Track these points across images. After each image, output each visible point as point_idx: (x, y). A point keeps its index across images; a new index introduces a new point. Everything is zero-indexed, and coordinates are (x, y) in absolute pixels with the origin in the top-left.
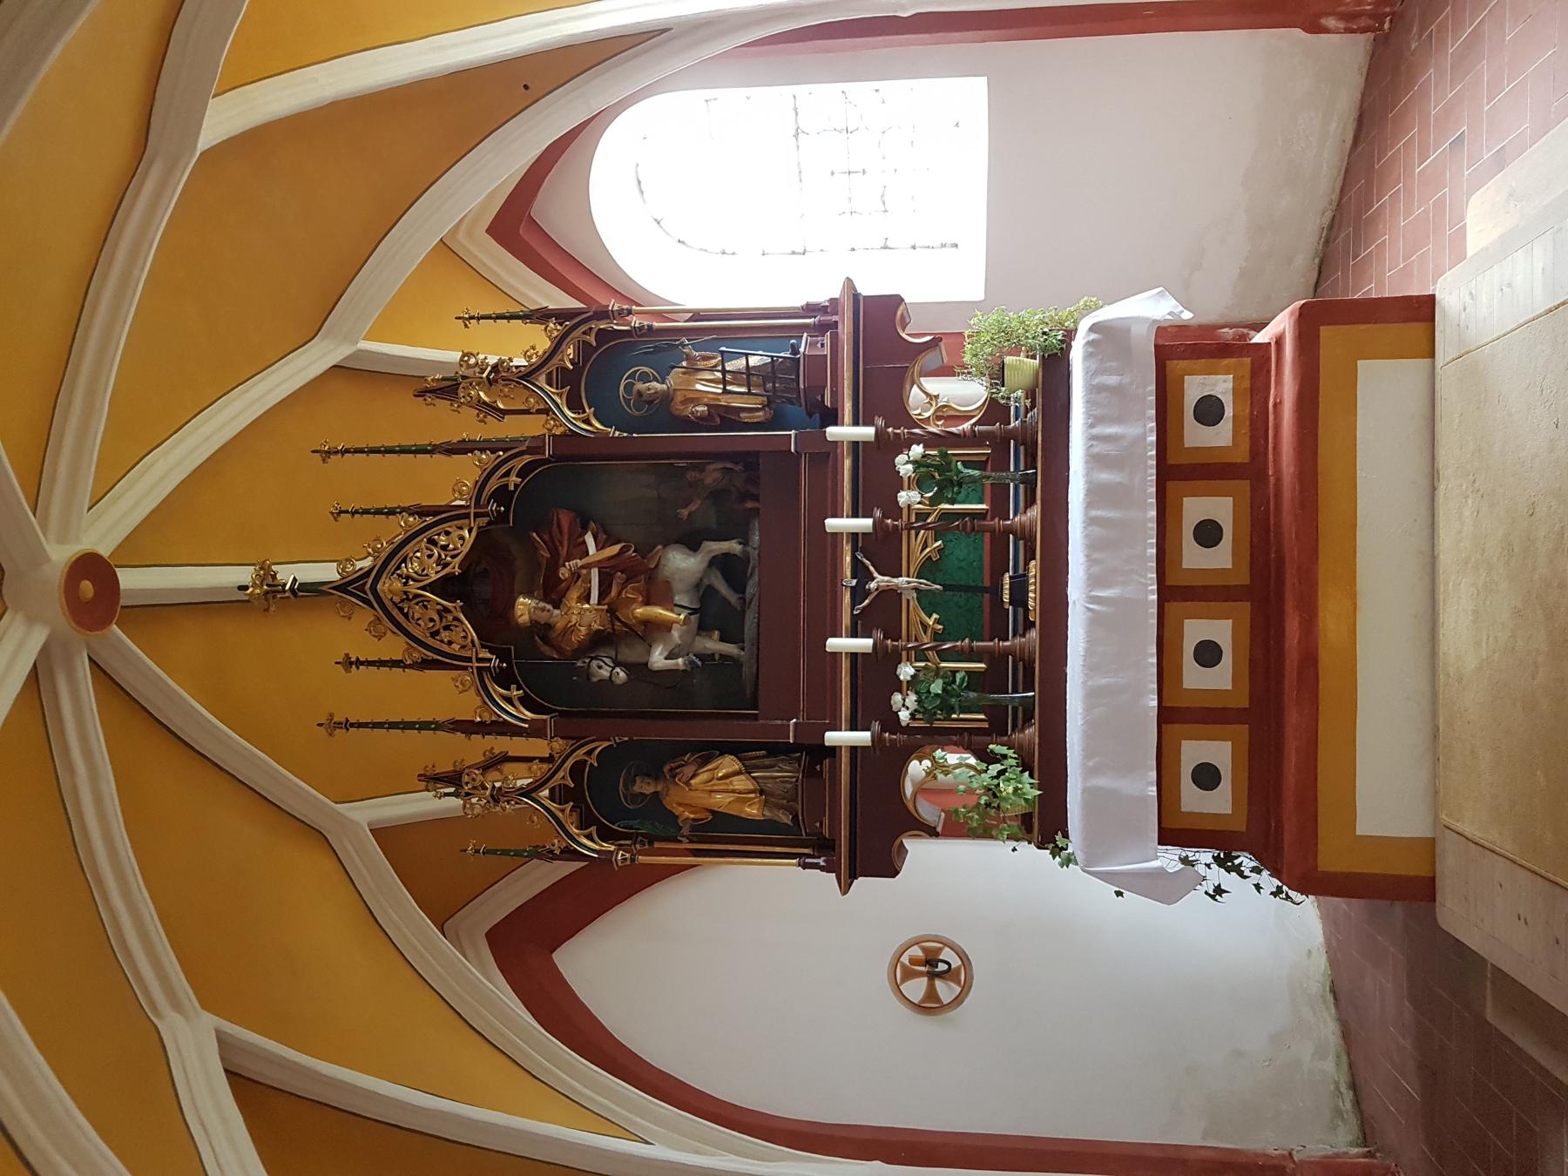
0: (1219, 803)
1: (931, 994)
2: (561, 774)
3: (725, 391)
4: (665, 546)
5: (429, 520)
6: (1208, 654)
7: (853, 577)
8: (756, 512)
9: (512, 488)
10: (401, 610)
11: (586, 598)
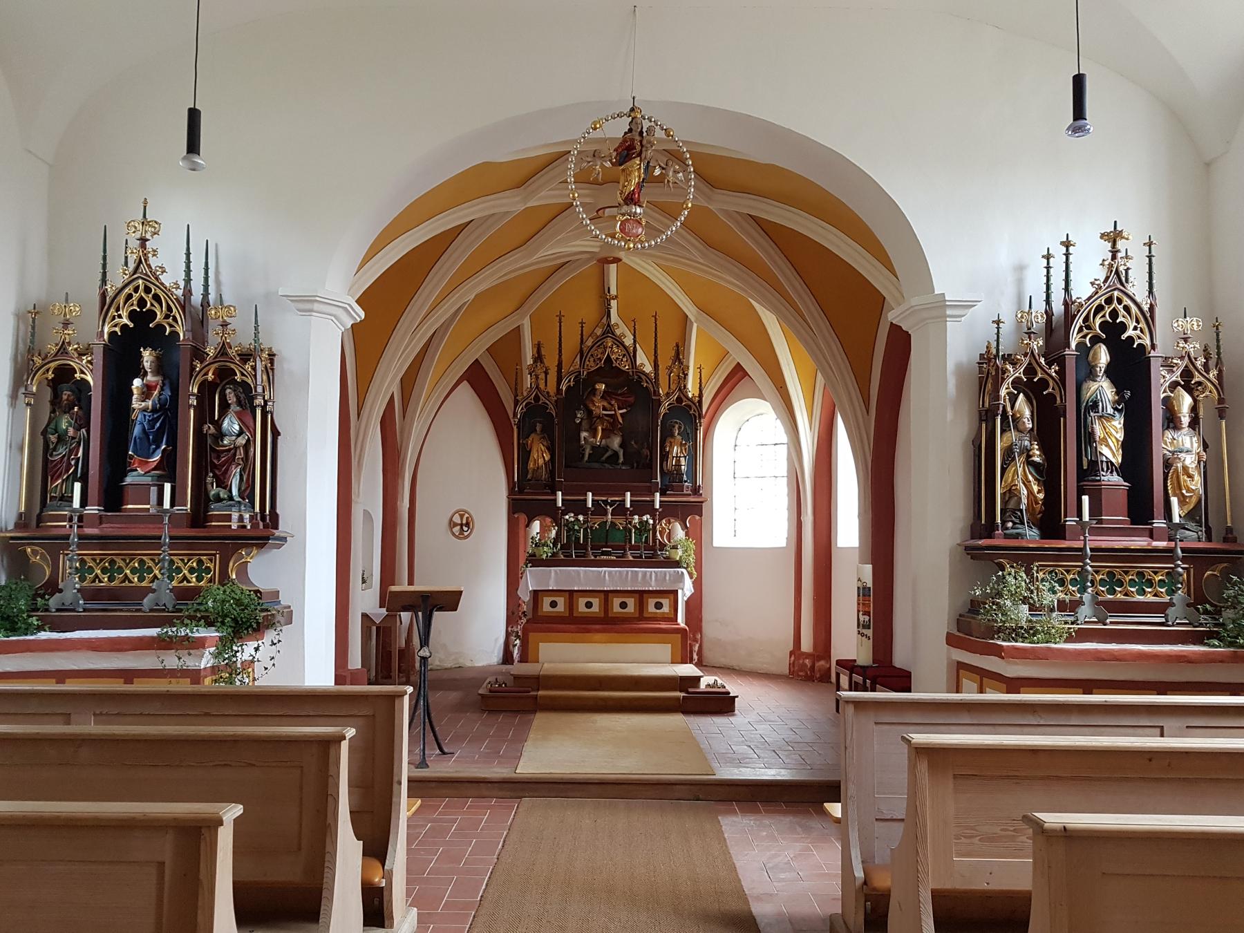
0: (546, 607)
1: (456, 524)
3: (673, 457)
6: (589, 605)
8: (633, 467)
10: (601, 345)
11: (604, 409)
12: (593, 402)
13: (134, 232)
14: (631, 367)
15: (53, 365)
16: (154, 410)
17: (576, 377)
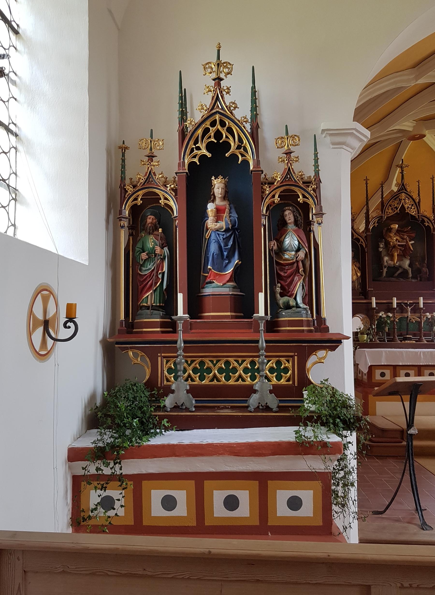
0: (377, 377)
2: (357, 235)
4: (410, 259)
5: (417, 204)
7: (410, 303)
9: (425, 224)
10: (397, 198)
12: (391, 237)
13: (211, 73)
14: (417, 213)
15: (141, 193)
16: (227, 230)
17: (379, 220)
